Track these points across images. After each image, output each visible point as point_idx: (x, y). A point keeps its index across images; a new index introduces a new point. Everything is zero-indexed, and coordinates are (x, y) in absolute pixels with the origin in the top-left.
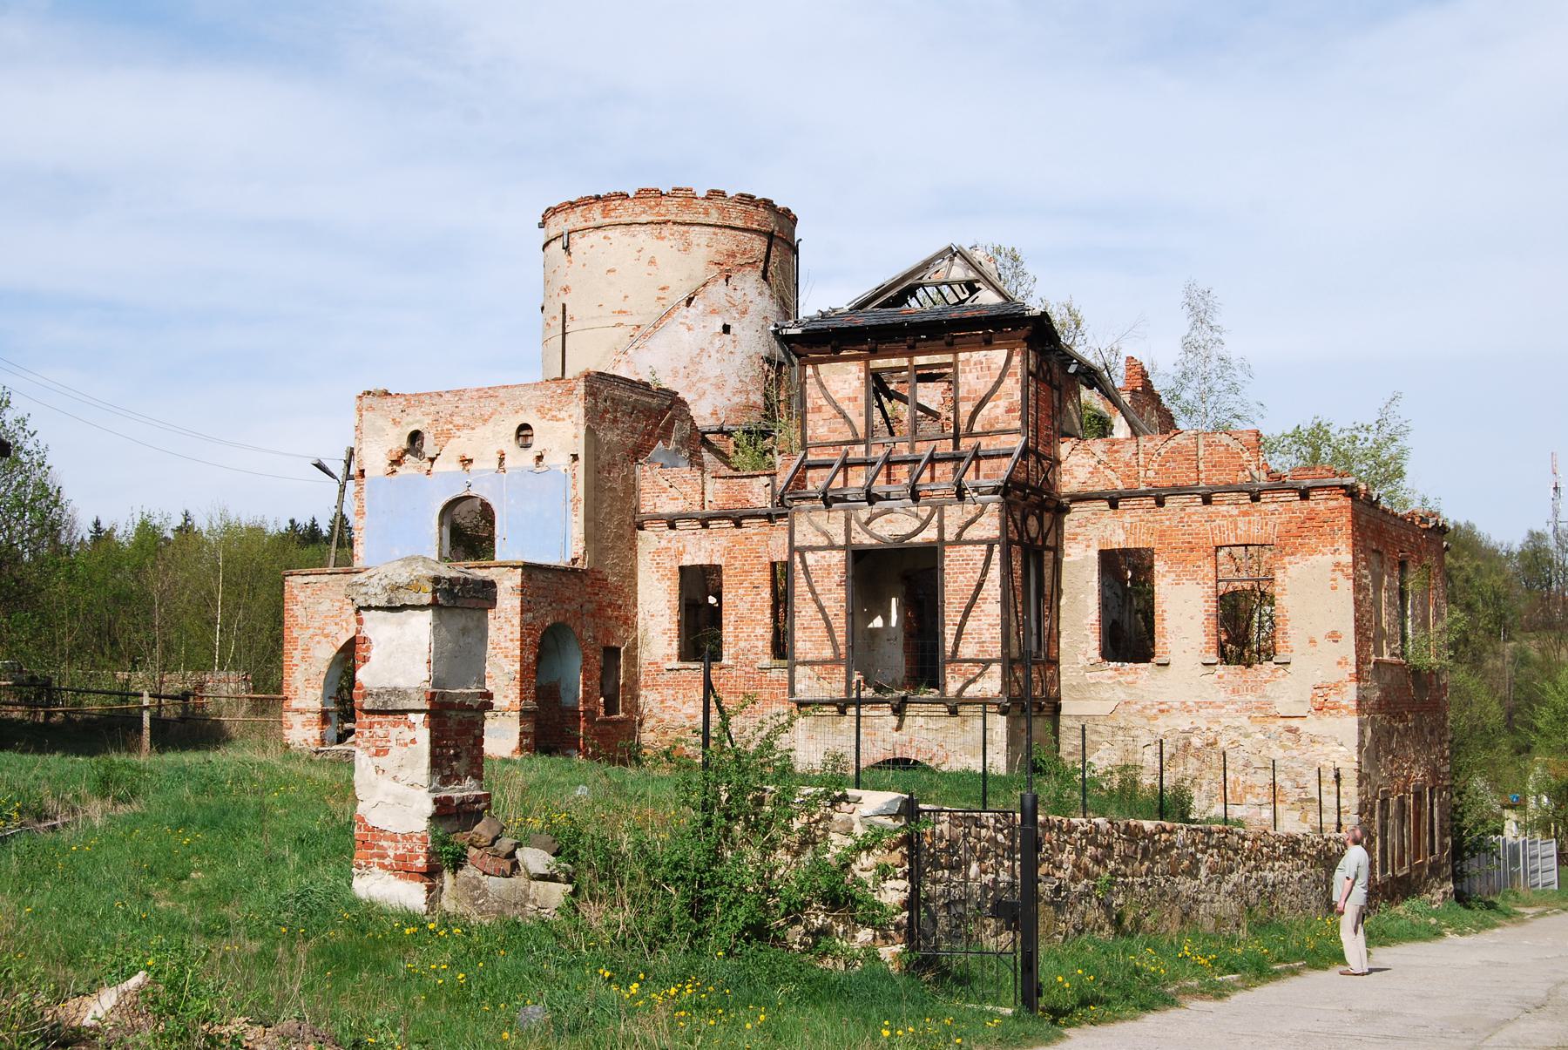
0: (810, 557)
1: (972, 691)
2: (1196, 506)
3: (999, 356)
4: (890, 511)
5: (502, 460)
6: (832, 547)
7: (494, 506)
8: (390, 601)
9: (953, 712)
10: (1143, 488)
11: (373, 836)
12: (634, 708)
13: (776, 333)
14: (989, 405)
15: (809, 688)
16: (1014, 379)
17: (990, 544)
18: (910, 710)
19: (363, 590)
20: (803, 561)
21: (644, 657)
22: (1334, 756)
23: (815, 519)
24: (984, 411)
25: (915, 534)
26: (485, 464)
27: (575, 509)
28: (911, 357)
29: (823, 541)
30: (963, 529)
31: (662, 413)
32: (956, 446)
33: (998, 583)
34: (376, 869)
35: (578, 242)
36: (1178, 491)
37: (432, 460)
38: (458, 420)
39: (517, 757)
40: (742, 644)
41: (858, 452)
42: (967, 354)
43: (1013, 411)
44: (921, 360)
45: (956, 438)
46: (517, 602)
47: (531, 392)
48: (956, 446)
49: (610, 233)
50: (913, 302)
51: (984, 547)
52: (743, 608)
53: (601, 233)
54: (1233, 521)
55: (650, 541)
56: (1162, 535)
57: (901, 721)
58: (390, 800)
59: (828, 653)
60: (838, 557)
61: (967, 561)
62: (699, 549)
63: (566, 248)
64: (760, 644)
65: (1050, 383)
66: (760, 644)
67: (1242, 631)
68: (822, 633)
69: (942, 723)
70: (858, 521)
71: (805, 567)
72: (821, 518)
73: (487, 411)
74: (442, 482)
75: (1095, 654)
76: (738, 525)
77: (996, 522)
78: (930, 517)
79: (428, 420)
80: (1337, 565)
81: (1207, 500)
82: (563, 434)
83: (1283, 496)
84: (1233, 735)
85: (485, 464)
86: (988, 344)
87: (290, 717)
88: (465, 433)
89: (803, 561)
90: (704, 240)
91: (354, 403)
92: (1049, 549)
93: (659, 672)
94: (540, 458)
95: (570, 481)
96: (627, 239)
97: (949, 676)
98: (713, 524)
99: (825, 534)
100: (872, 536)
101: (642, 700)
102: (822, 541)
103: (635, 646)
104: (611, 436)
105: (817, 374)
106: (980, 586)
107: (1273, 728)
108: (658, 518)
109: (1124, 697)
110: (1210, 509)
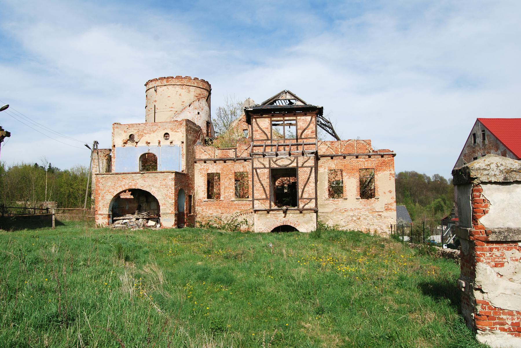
0: (258, 171)
1: (307, 207)
2: (354, 159)
3: (309, 118)
4: (282, 158)
5: (159, 143)
6: (265, 168)
7: (157, 156)
8: (505, 178)
9: (301, 212)
10: (340, 154)
11: (495, 313)
12: (194, 212)
13: (245, 110)
15: (259, 206)
18: (288, 212)
19: (486, 172)
20: (256, 171)
21: (197, 198)
22: (390, 221)
23: (260, 160)
24: (305, 132)
25: (289, 164)
26: (154, 144)
27: (183, 157)
28: (284, 118)
29: (262, 166)
30: (304, 163)
31: (198, 132)
32: (297, 142)
33: (314, 178)
34: (498, 331)
35: (159, 89)
36: (350, 155)
37: (137, 143)
38: (145, 131)
39: (174, 227)
40: (226, 194)
41: (269, 143)
44: (286, 118)
45: (297, 139)
46: (173, 183)
47: (169, 124)
48: (297, 142)
49: (168, 87)
50: (275, 104)
52: (227, 184)
53: (166, 87)
54: (364, 163)
55: (198, 166)
56: (345, 166)
57: (286, 215)
58: (508, 292)
59: (264, 197)
60: (267, 171)
61: (305, 172)
62: (213, 168)
63: (156, 91)
64: (232, 194)
66: (232, 194)
67: (367, 191)
68: (262, 191)
69: (298, 215)
70: (273, 161)
71: (257, 173)
72: (262, 160)
73: (154, 129)
74: (141, 149)
75: (327, 196)
76: (225, 162)
77: (313, 161)
78: (294, 160)
79: (136, 131)
80: (391, 174)
81: (357, 157)
82: (179, 136)
83: (377, 157)
84: (364, 217)
85: (154, 144)
86: (305, 115)
87: (97, 216)
88: (148, 135)
89: (256, 171)
90: (193, 90)
91: (112, 126)
93: (201, 202)
94: (171, 143)
95: (181, 149)
97: (300, 203)
98: (217, 162)
99: (263, 164)
100: (277, 165)
101: (196, 209)
103: (194, 195)
104: (190, 137)
105: (256, 121)
106: (309, 178)
107: (375, 215)
108: (201, 160)
109: (335, 207)
110: (358, 159)
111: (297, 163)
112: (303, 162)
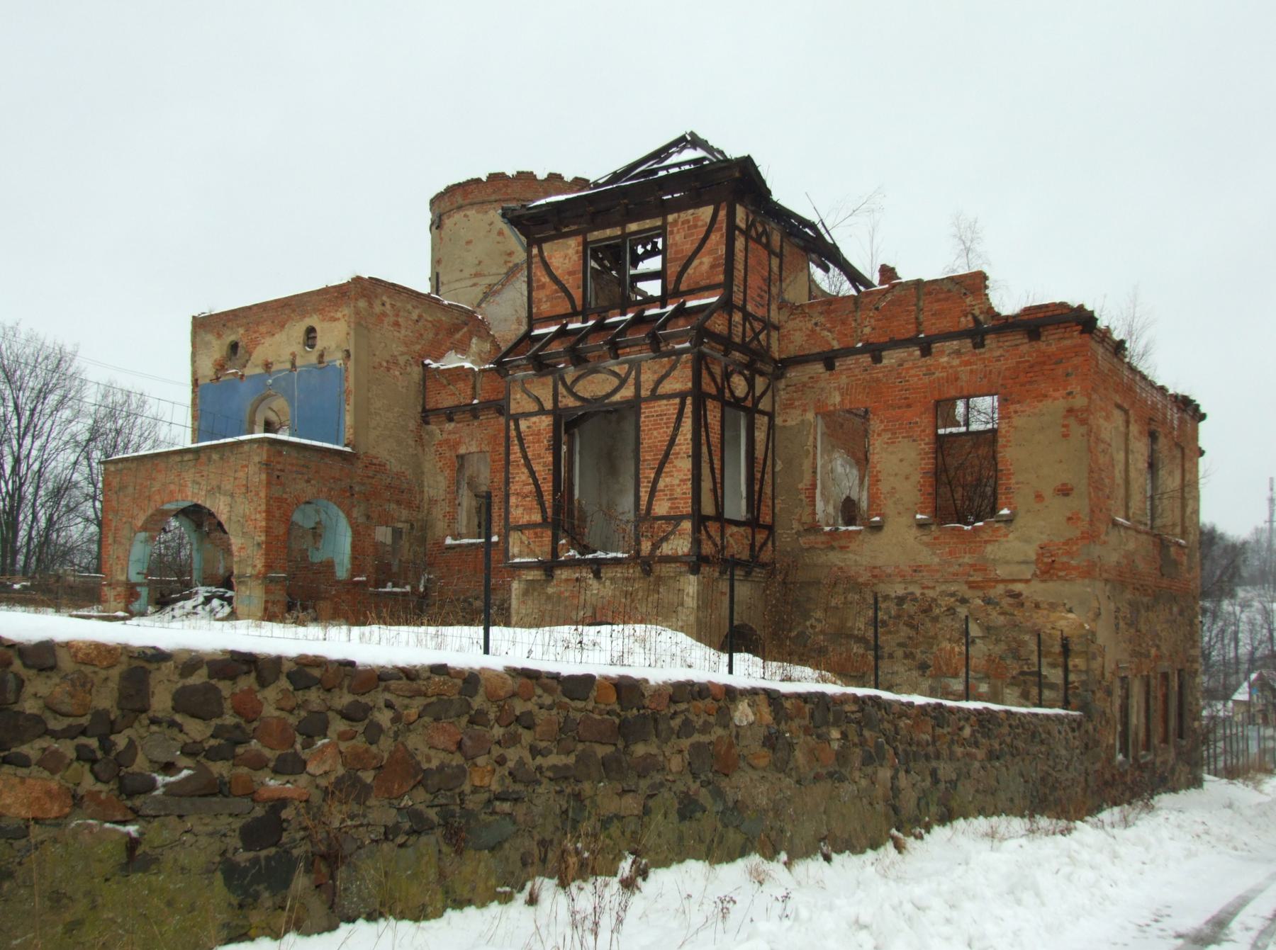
1: (666, 549)
6: (542, 411)
14: (696, 262)
16: (718, 235)
17: (682, 396)
24: (690, 271)
28: (623, 225)
33: (689, 436)
42: (676, 215)
43: (719, 265)
51: (677, 401)
59: (537, 517)
60: (545, 422)
65: (767, 246)
70: (564, 384)
77: (689, 372)
78: (628, 374)
80: (1070, 411)
92: (763, 413)
96: (480, 216)
99: (537, 400)
102: (533, 407)
105: (541, 251)
110: (929, 361)
111: (638, 386)
112: (656, 377)
